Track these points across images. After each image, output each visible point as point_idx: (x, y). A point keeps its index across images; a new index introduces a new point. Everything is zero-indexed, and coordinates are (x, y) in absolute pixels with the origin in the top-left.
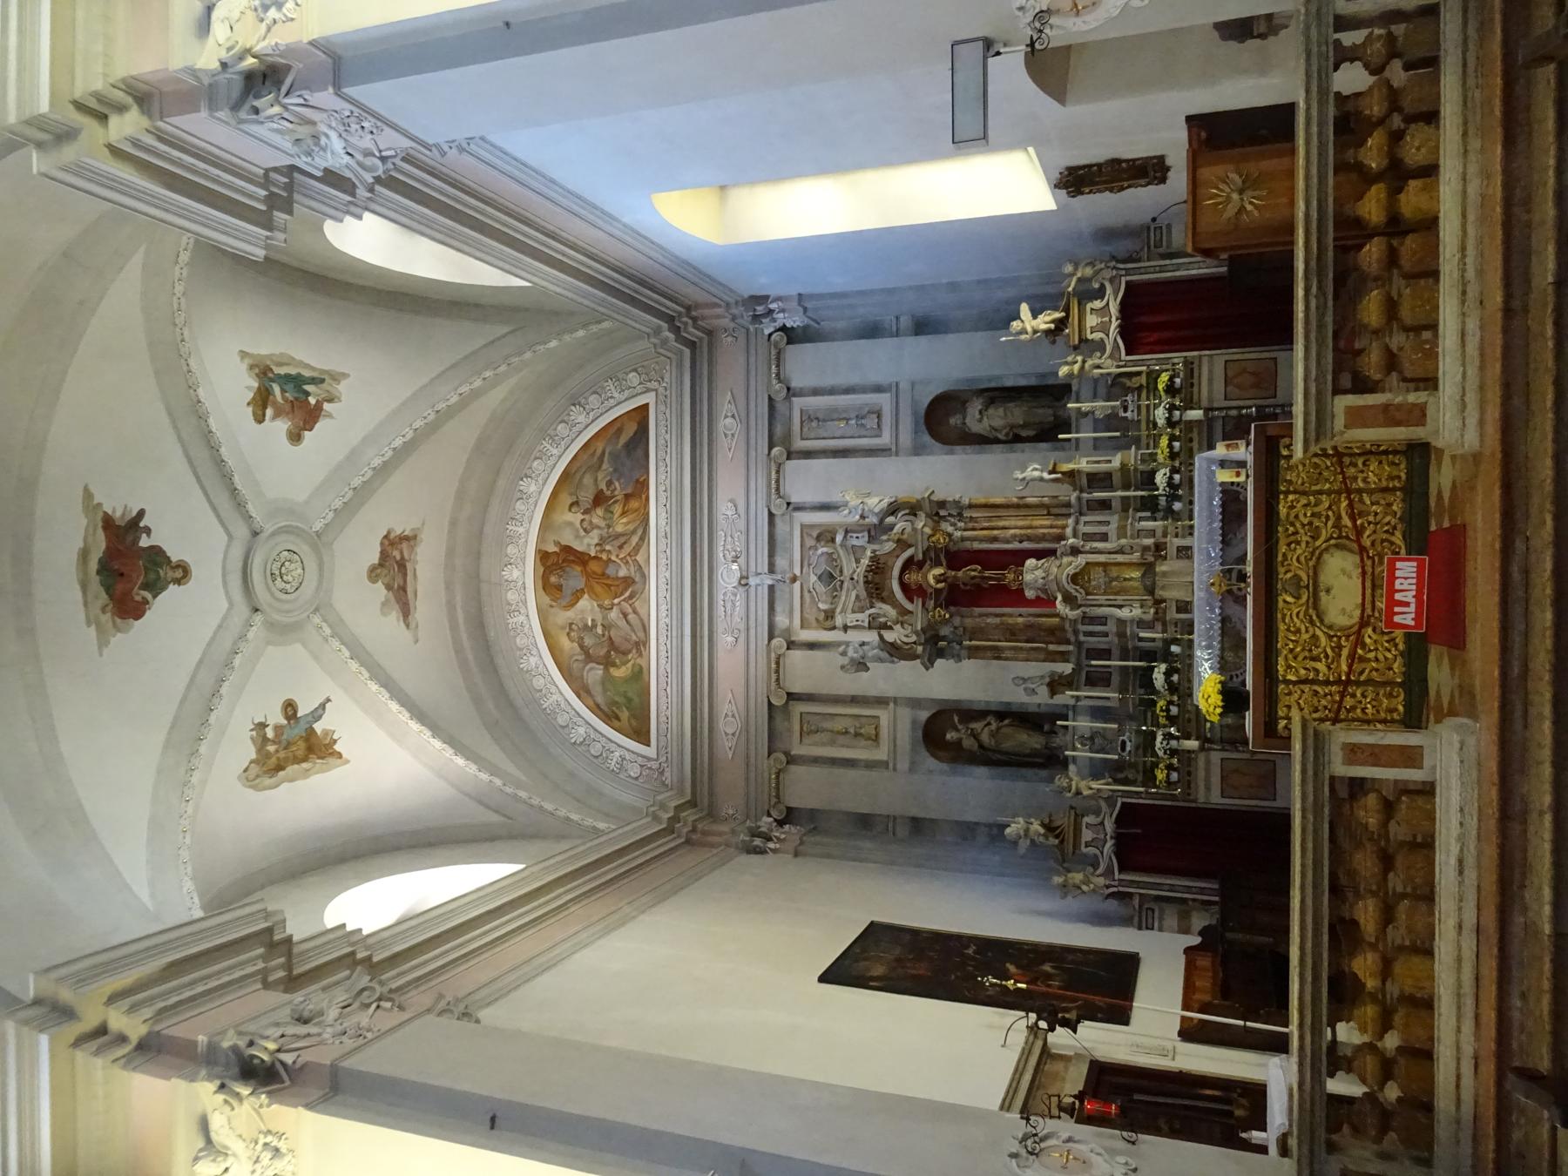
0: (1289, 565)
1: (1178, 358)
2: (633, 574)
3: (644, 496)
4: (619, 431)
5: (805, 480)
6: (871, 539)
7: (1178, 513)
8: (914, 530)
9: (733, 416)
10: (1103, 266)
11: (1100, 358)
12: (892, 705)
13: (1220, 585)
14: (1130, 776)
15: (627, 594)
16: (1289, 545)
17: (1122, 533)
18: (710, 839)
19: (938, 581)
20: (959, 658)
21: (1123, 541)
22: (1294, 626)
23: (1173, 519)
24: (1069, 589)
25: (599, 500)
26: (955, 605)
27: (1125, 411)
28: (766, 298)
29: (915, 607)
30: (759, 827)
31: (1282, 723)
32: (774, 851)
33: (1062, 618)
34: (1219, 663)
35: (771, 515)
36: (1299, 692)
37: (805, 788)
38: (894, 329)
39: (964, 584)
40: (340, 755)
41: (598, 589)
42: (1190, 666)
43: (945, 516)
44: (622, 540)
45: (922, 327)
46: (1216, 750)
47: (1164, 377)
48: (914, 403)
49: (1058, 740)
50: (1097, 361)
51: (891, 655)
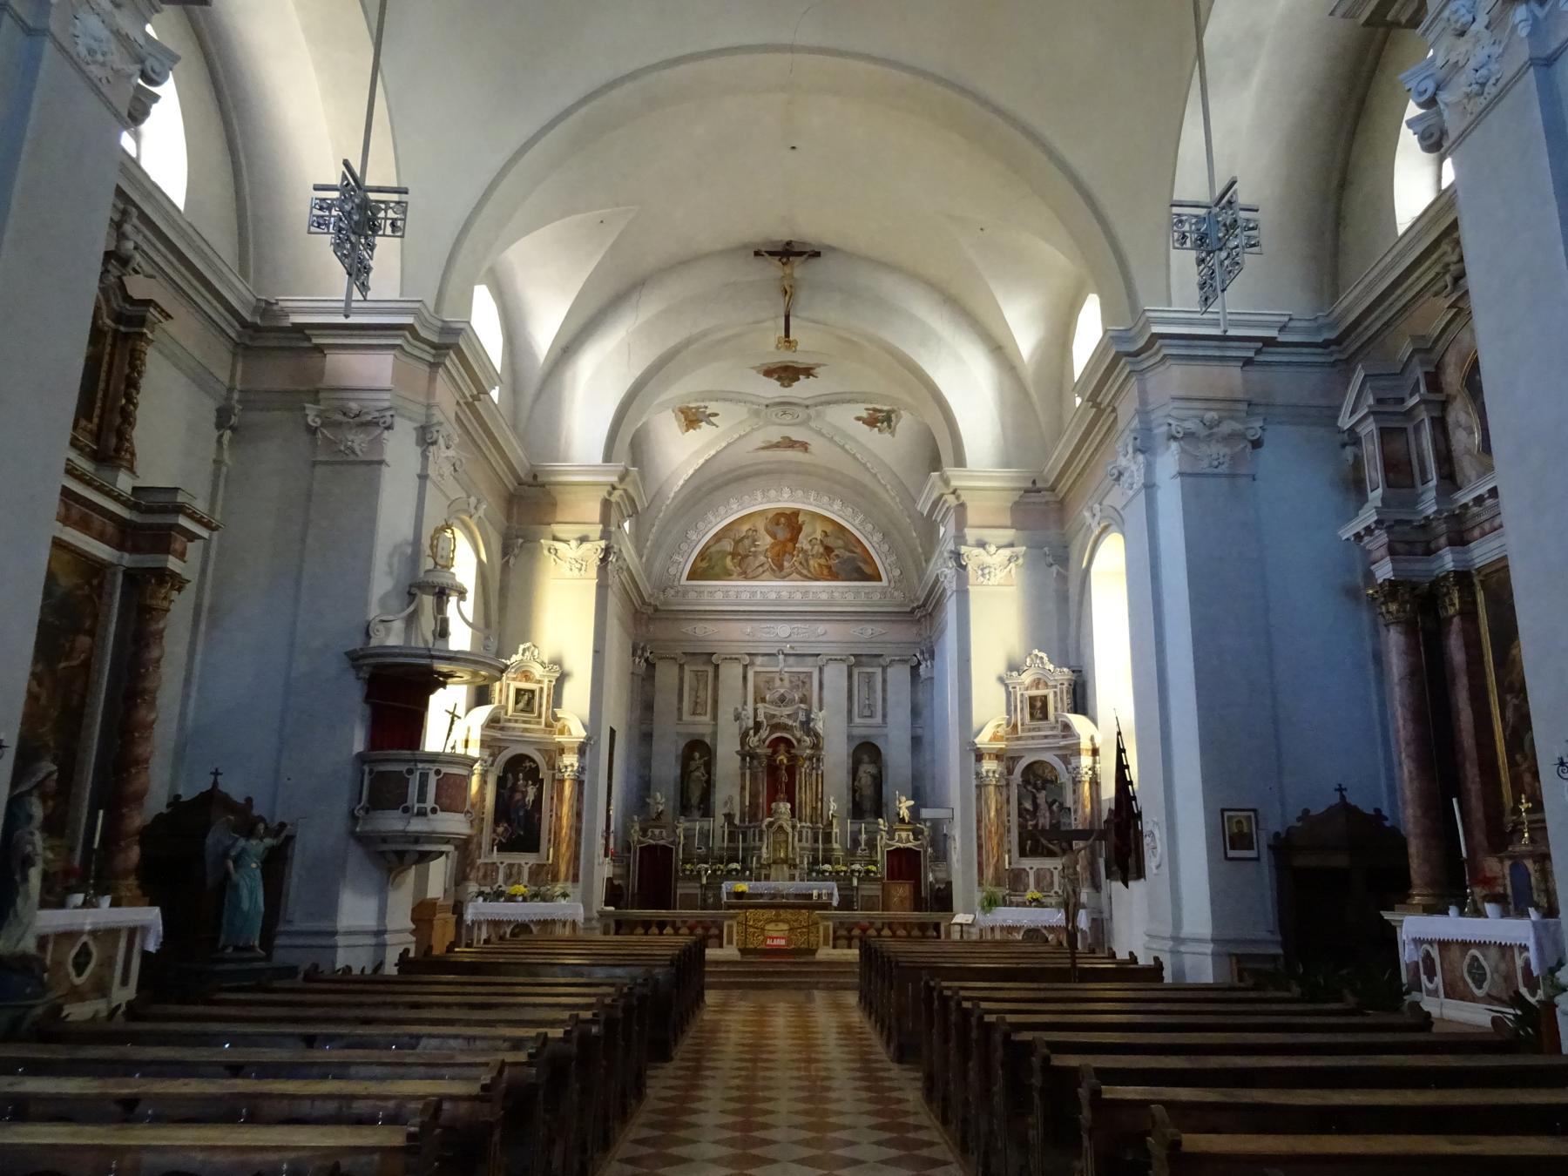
4: (866, 562)
5: (835, 677)
17: (802, 849)
25: (828, 550)
28: (933, 659)
37: (666, 675)
40: (687, 431)
41: (777, 548)
45: (916, 742)
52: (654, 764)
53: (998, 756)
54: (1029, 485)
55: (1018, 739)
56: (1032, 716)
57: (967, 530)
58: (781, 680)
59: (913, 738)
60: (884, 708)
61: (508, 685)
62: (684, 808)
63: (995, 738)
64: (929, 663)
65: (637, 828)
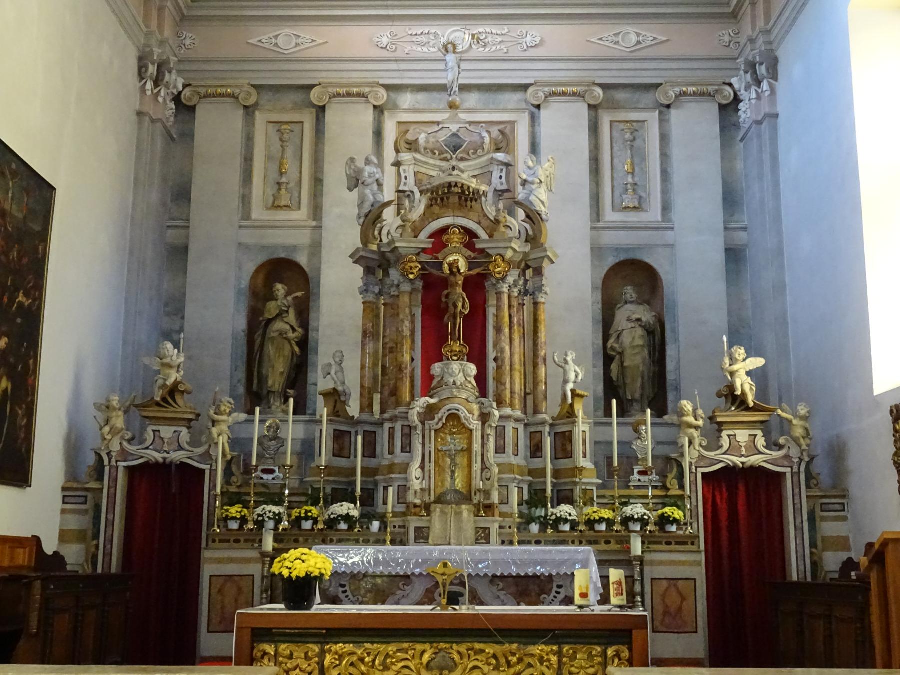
0: (469, 656)
1: (699, 528)
6: (499, 194)
7: (527, 529)
8: (510, 240)
9: (639, 43)
10: (804, 447)
11: (701, 445)
12: (314, 224)
13: (443, 575)
14: (234, 479)
16: (495, 656)
17: (505, 468)
18: (154, 14)
19: (451, 265)
20: (364, 291)
21: (496, 470)
22: (393, 664)
23: (520, 524)
24: (443, 411)
26: (424, 288)
27: (640, 473)
29: (424, 240)
30: (170, 72)
31: (270, 649)
32: (143, 90)
33: (410, 404)
34: (359, 573)
35: (525, 88)
36: (309, 669)
38: (733, 225)
39: (447, 296)
42: (357, 542)
43: (524, 275)
46: (263, 570)
47: (678, 514)
48: (650, 247)
49: (278, 404)
50: (697, 442)
51: (367, 216)
52: (190, 310)
59: (728, 250)
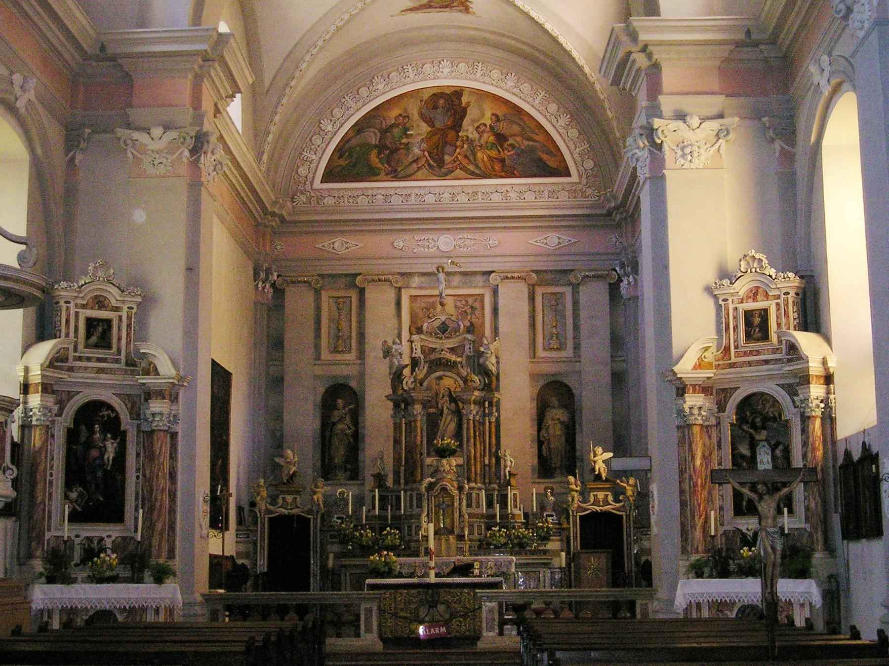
2: (447, 167)
3: (503, 174)
4: (549, 153)
9: (559, 243)
15: (432, 162)
21: (467, 517)
25: (501, 138)
28: (637, 274)
32: (257, 286)
41: (436, 137)
44: (471, 158)
45: (618, 379)
52: (286, 417)
53: (705, 389)
54: (741, 36)
55: (732, 365)
56: (749, 336)
57: (662, 99)
58: (442, 304)
60: (576, 337)
61: (77, 314)
62: (327, 471)
63: (700, 365)
64: (631, 279)
65: (264, 494)
